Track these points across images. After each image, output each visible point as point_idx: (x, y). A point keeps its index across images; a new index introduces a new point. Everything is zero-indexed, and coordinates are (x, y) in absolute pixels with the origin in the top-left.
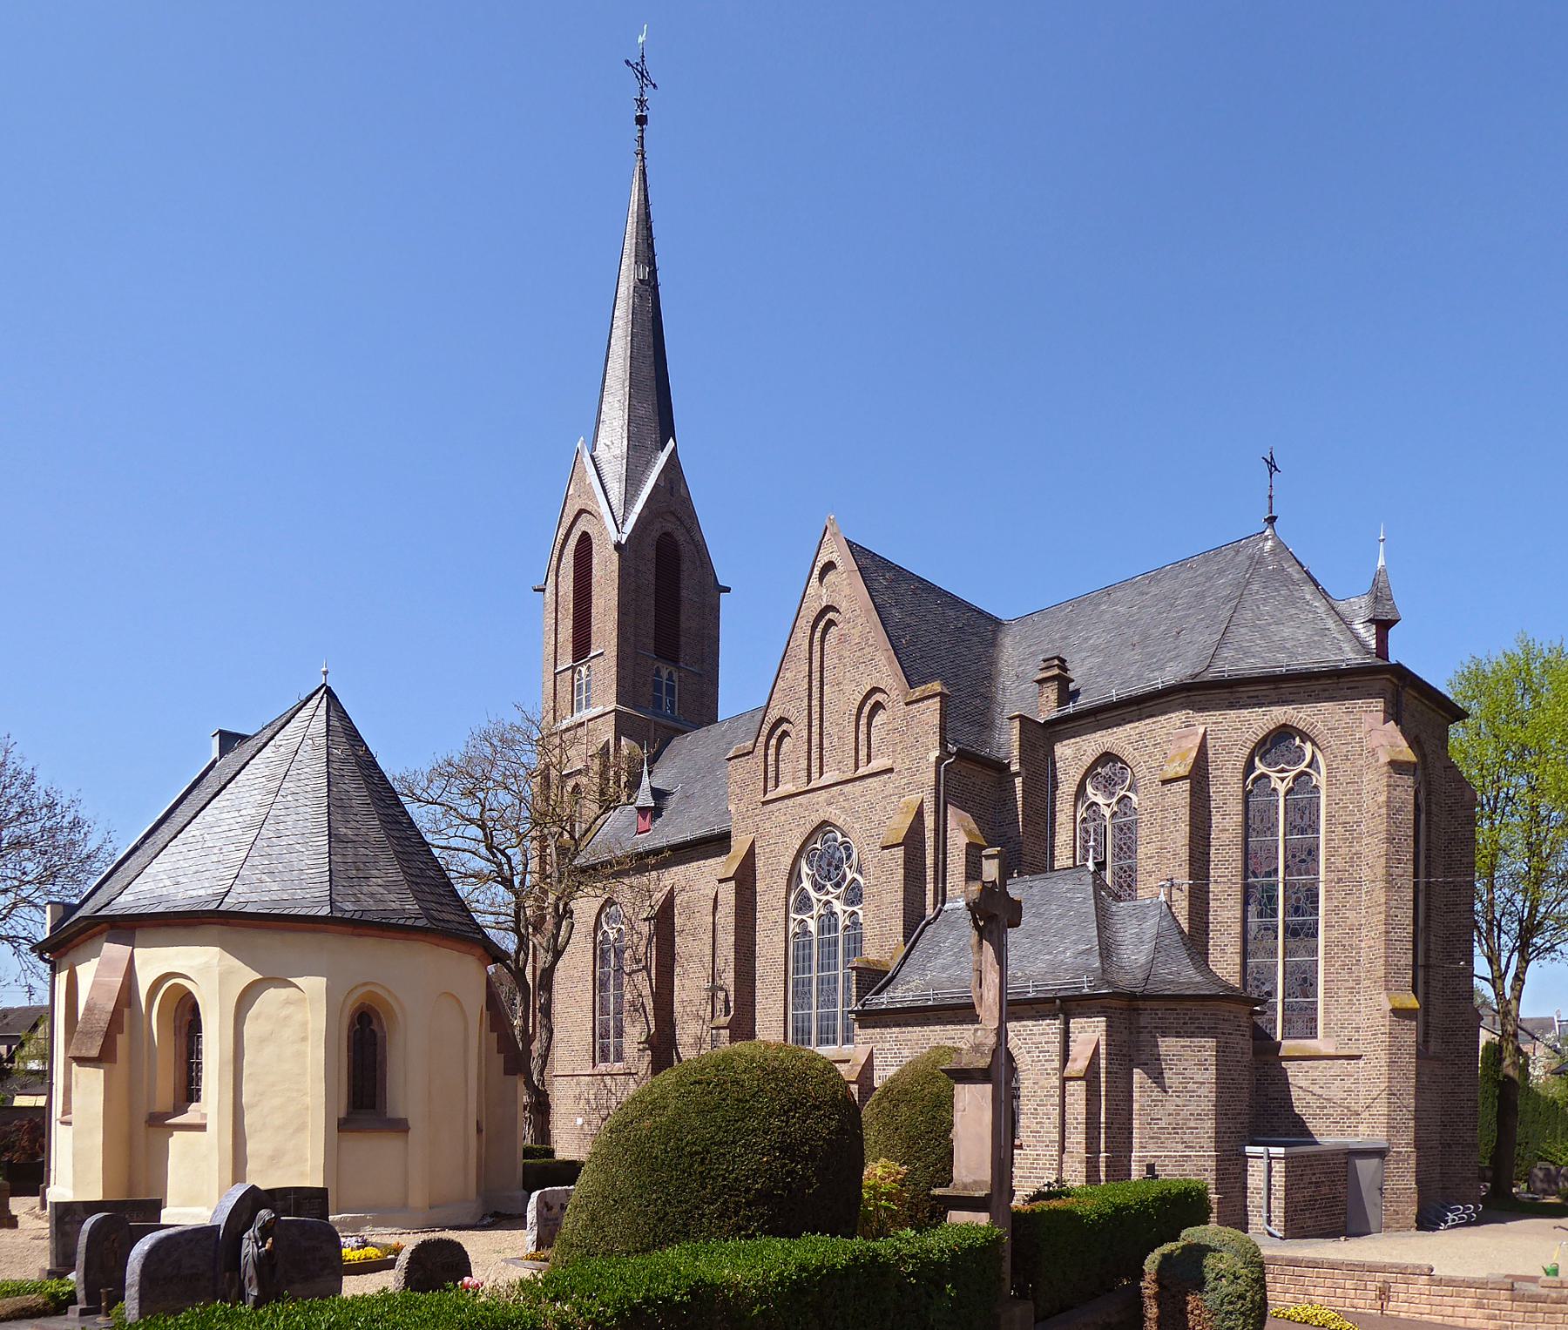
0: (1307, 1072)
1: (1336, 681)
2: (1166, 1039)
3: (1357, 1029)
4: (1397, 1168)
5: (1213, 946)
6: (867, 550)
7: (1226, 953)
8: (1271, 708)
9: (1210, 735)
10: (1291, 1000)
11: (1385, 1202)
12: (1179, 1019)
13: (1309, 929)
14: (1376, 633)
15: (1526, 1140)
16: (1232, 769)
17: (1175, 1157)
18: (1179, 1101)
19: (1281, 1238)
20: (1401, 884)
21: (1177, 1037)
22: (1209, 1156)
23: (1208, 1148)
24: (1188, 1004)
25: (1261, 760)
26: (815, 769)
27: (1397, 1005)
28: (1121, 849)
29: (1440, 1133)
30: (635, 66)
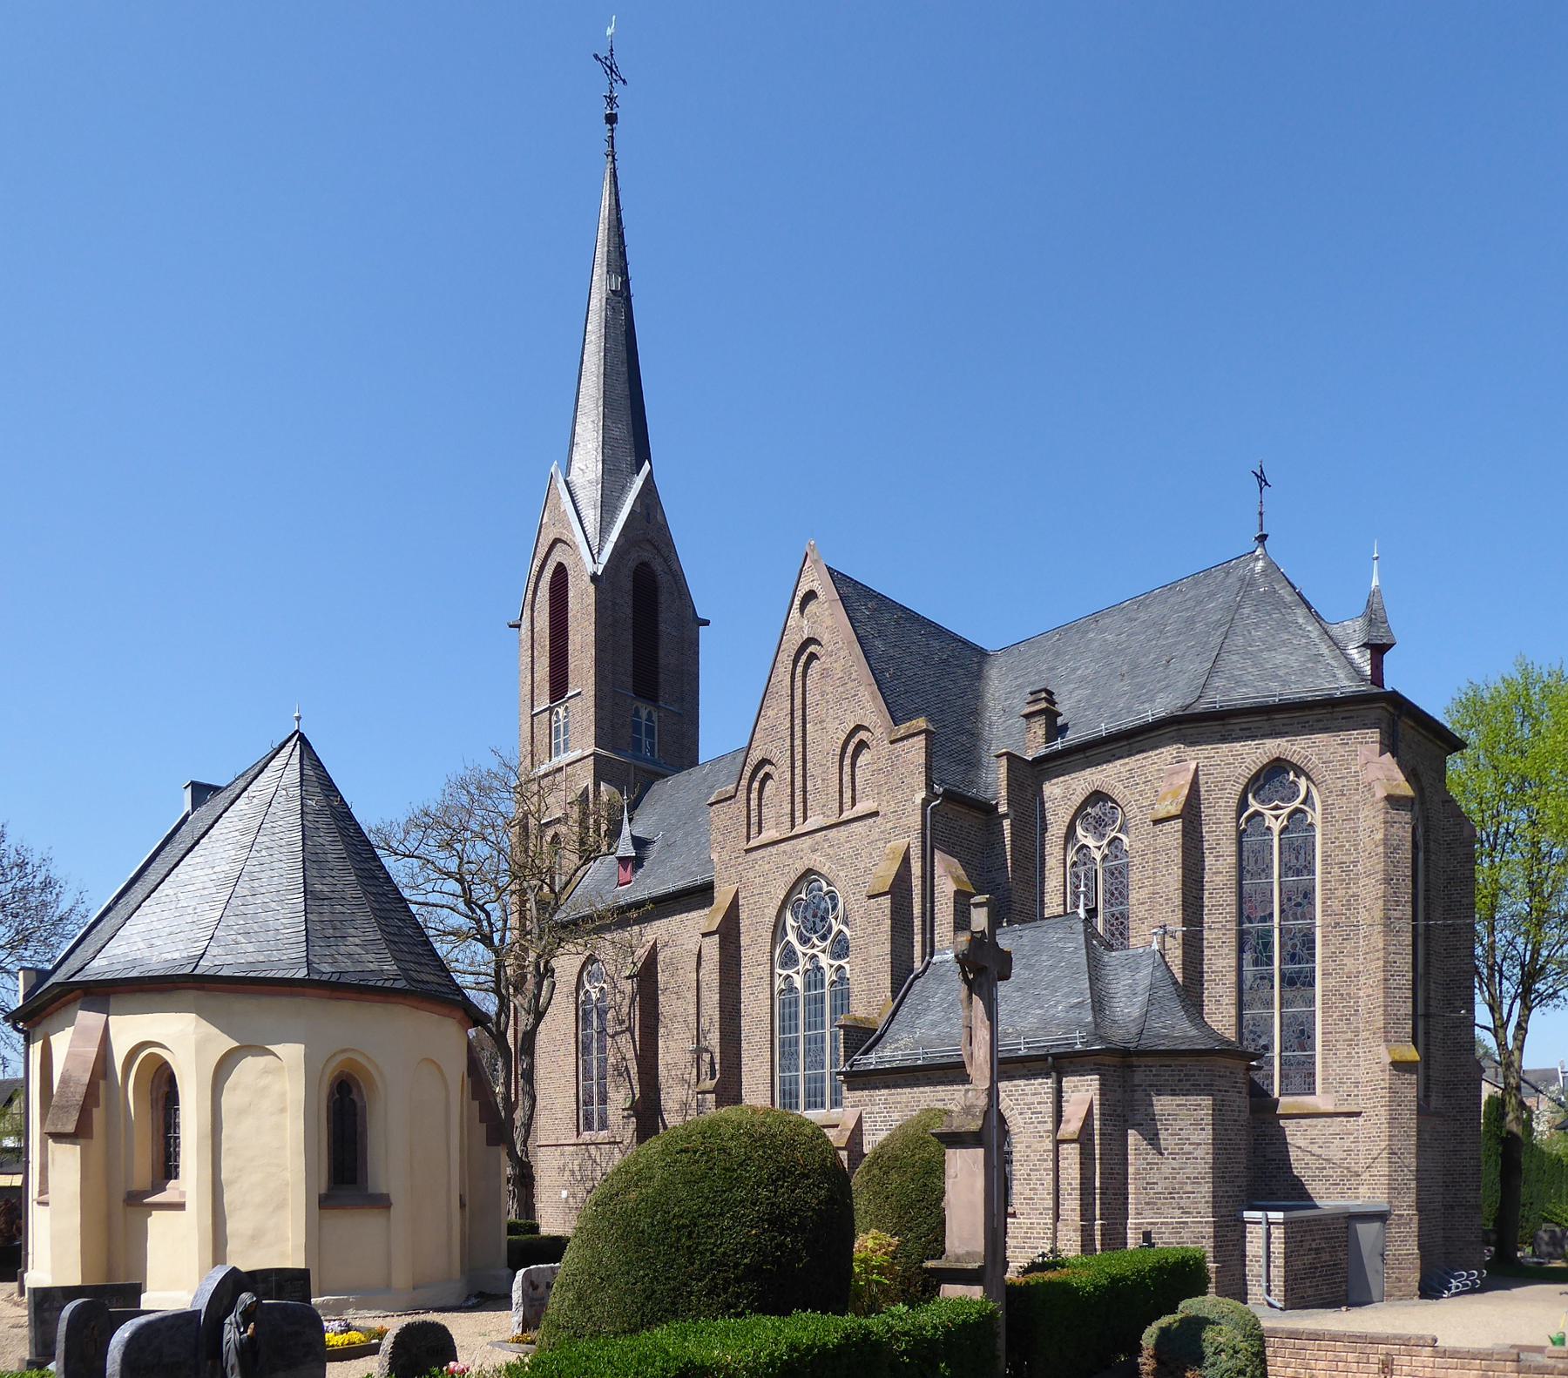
0: (1306, 1130)
2: (1162, 1097)
4: (1399, 1232)
9: (1202, 770)
10: (1288, 1054)
11: (1387, 1269)
14: (1371, 659)
15: (1531, 1201)
16: (1226, 807)
17: (1172, 1223)
18: (1175, 1164)
19: (1281, 1309)
22: (1206, 1222)
24: (1183, 1060)
25: (1254, 797)
26: (799, 814)
27: (1397, 1058)
29: (1442, 1194)
30: (604, 60)
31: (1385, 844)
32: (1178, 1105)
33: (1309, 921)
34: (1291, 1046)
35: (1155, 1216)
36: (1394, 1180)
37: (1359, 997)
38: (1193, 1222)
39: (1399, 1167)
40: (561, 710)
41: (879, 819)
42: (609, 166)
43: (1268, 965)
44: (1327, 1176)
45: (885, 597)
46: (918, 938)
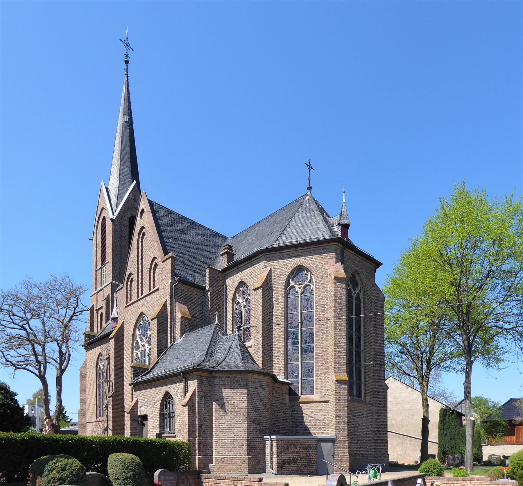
0: (310, 408)
1: (317, 246)
2: (226, 390)
3: (328, 390)
4: (340, 447)
5: (275, 357)
6: (161, 206)
7: (279, 360)
8: (295, 259)
9: (273, 270)
10: (305, 379)
11: (335, 461)
12: (231, 381)
13: (311, 349)
14: (341, 230)
15: (455, 446)
16: (281, 284)
17: (230, 439)
18: (232, 416)
19: (275, 474)
20: (341, 328)
21: (230, 389)
22: (244, 439)
23: (244, 436)
24: (235, 375)
25: (292, 280)
26: (140, 292)
27: (338, 379)
28: (247, 320)
29: (374, 435)
30: (124, 42)
31: (334, 296)
32: (233, 393)
33: (312, 328)
34: (305, 376)
35: (223, 436)
36: (338, 426)
37: (328, 356)
38: (239, 439)
39: (340, 421)
40: (104, 268)
41: (159, 291)
42: (126, 78)
43: (297, 345)
44: (317, 426)
45: (179, 214)
46: (169, 335)
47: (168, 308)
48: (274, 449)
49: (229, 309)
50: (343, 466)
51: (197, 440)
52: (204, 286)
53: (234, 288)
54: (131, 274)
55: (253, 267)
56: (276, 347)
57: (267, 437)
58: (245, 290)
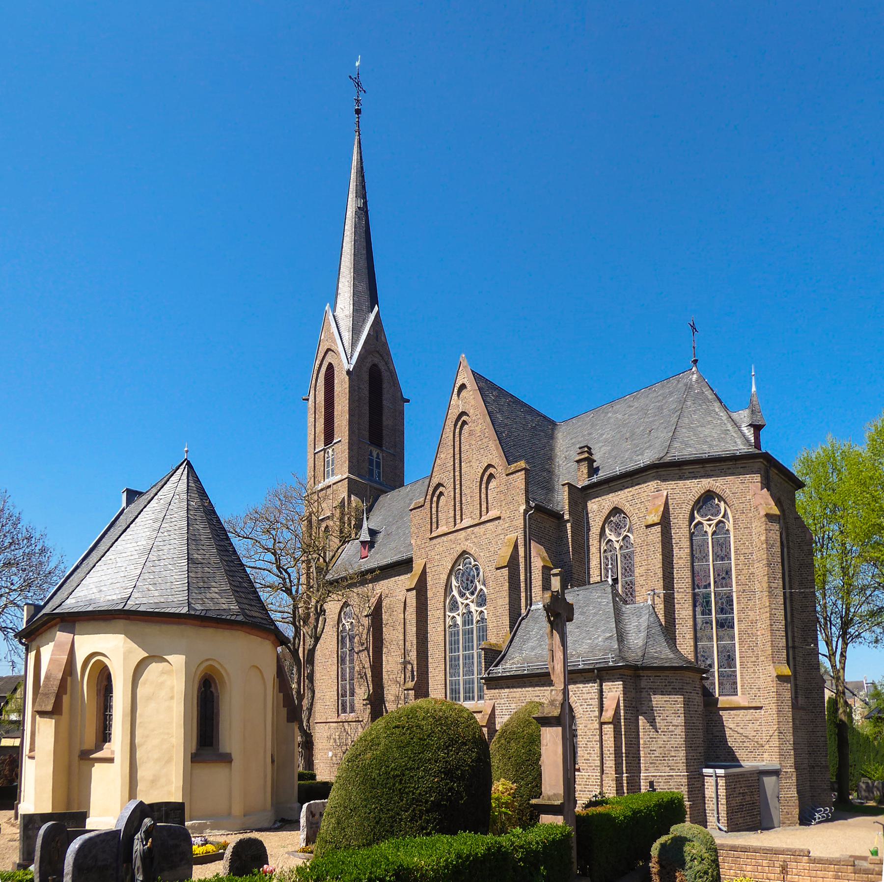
2: (656, 696)
4: (787, 783)
5: (679, 634)
8: (702, 480)
10: (722, 670)
13: (730, 622)
17: (665, 776)
19: (726, 832)
22: (683, 776)
24: (667, 673)
25: (698, 513)
26: (458, 517)
27: (779, 673)
28: (626, 570)
32: (665, 701)
33: (729, 588)
36: (782, 749)
37: (758, 636)
38: (676, 775)
40: (330, 451)
41: (501, 521)
43: (709, 615)
47: (519, 549)
48: (721, 791)
49: (593, 550)
50: (791, 814)
51: (624, 778)
52: (562, 513)
53: (602, 516)
54: (440, 485)
55: (637, 487)
56: (680, 619)
57: (706, 771)
58: (621, 522)
